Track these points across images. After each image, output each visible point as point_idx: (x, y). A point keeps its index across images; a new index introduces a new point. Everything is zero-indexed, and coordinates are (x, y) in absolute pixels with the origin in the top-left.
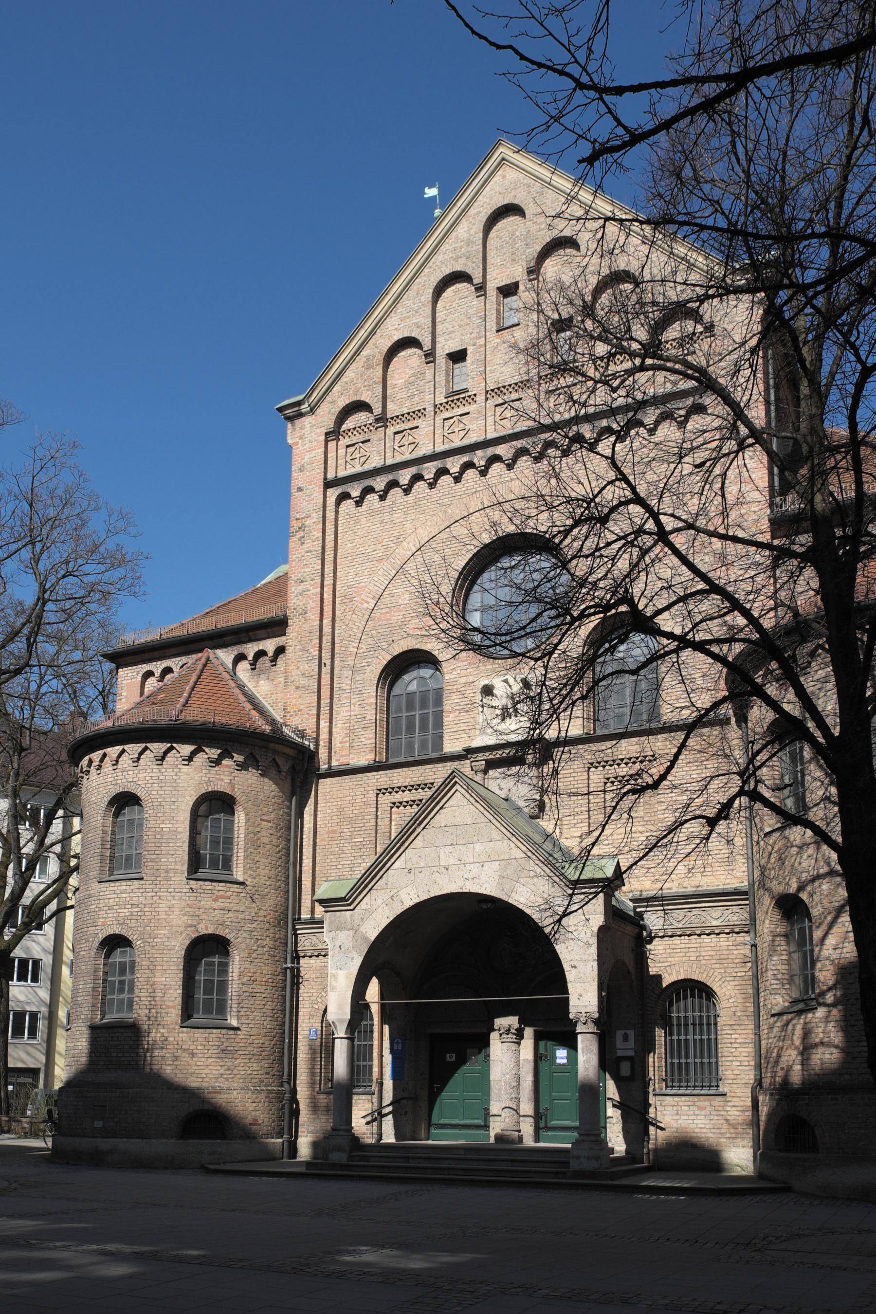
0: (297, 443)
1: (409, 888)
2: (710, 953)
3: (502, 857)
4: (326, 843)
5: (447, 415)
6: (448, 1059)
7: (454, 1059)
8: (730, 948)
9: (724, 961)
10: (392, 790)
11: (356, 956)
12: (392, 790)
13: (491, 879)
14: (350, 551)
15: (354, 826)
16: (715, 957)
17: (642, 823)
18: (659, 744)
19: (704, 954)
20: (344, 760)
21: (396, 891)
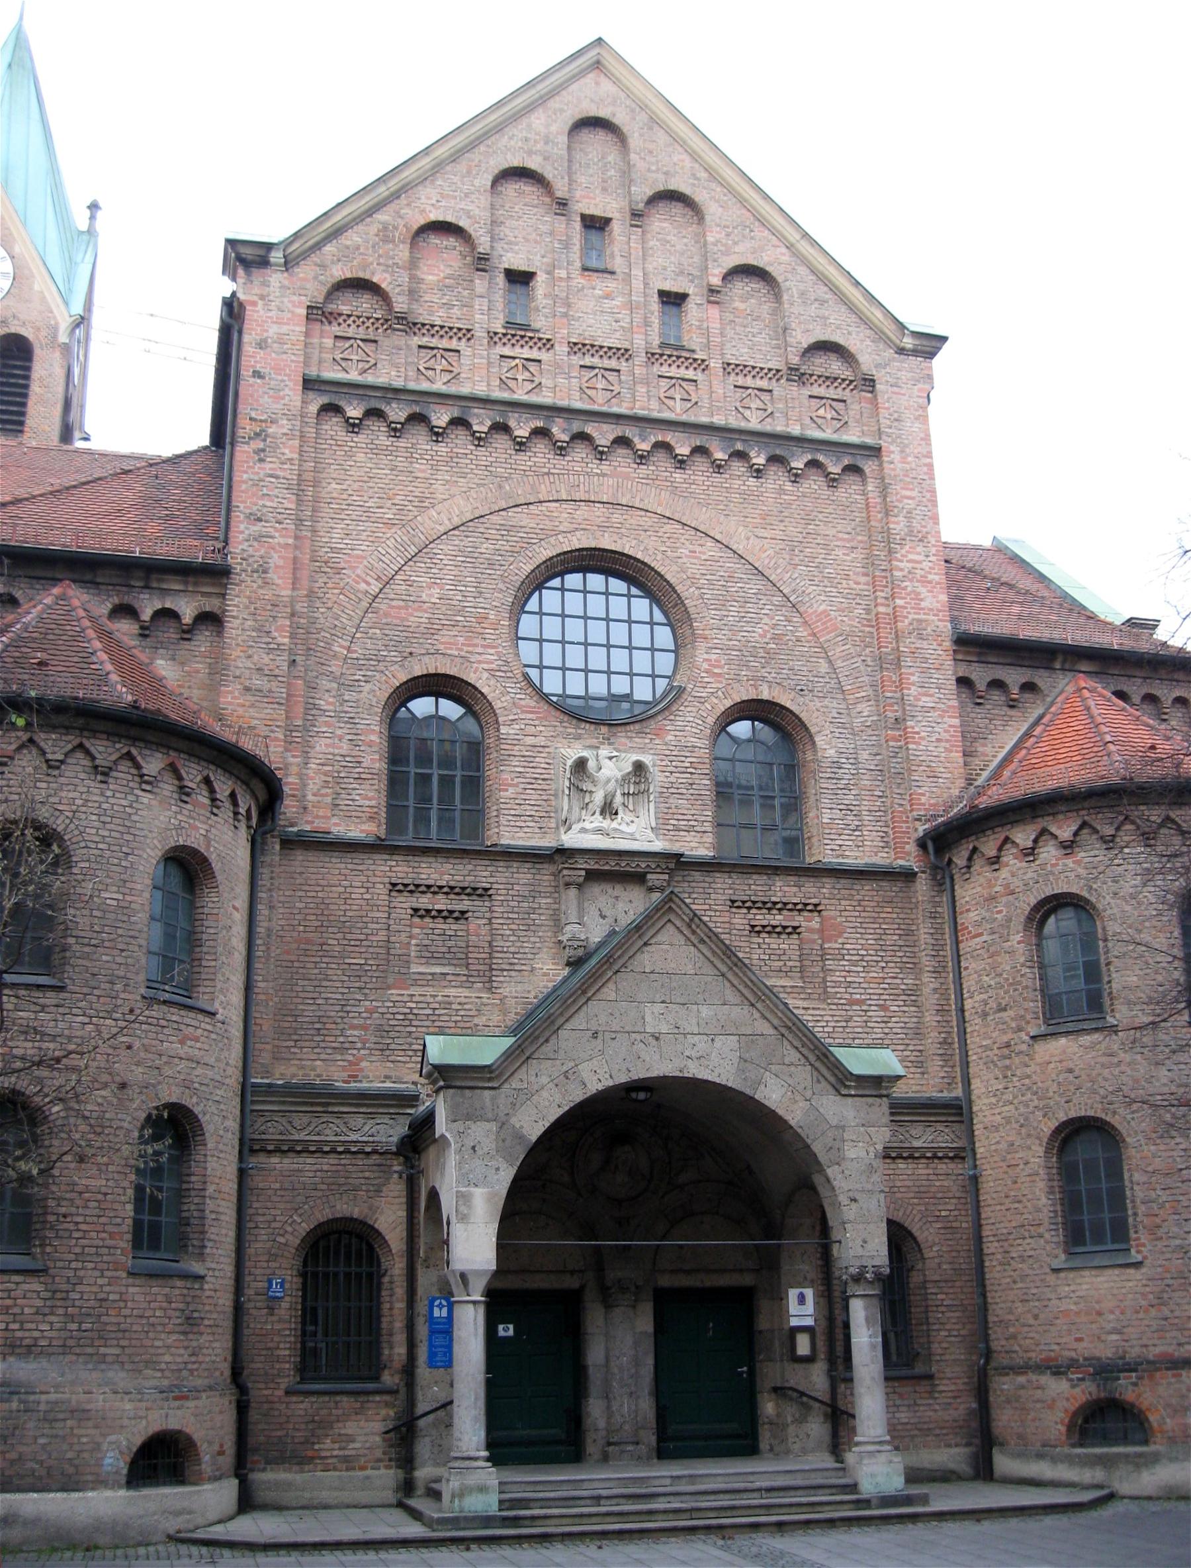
0: (254, 304)
2: (906, 1183)
3: (743, 1030)
4: (293, 958)
5: (507, 351)
6: (501, 1333)
7: (511, 1332)
8: (931, 1177)
10: (417, 889)
11: (503, 1165)
12: (417, 889)
13: (727, 1061)
14: (335, 495)
15: (348, 936)
17: (802, 996)
19: (899, 1184)
20: (320, 824)
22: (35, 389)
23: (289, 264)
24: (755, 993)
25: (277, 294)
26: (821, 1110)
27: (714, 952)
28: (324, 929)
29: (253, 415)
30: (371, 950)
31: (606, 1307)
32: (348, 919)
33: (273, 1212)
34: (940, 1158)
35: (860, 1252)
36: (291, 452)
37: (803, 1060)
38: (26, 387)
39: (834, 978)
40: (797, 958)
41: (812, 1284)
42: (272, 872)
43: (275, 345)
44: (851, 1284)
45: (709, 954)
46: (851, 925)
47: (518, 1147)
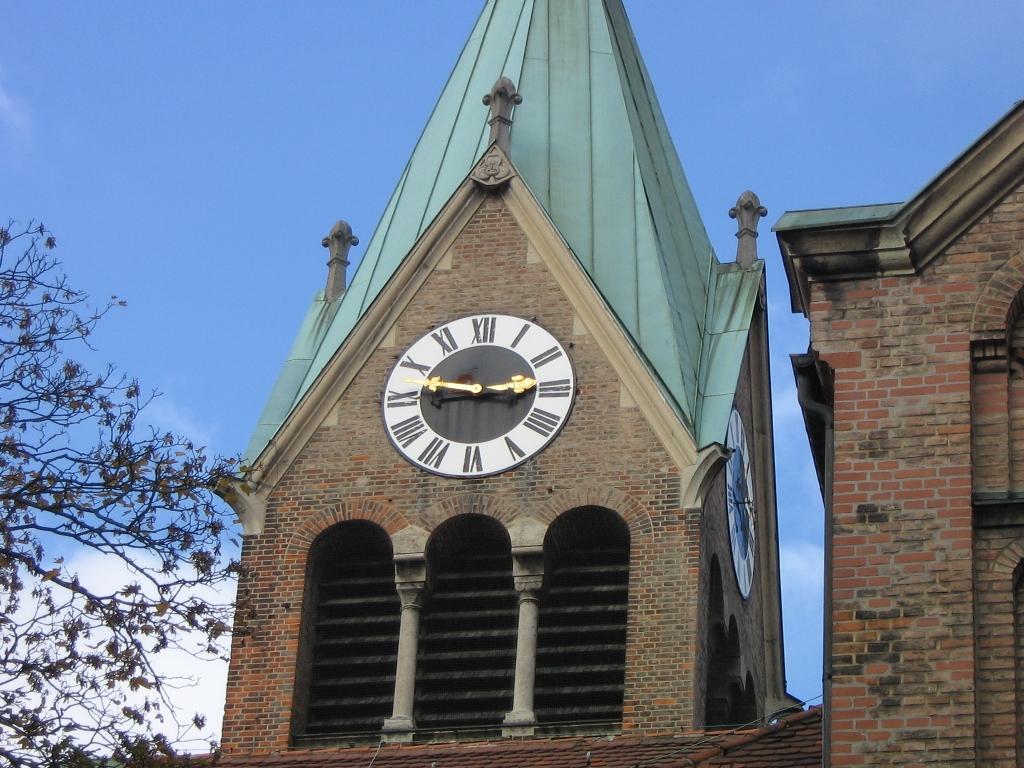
0: (852, 360)
22: (641, 618)
23: (920, 260)
25: (901, 329)
29: (865, 607)
36: (956, 676)
38: (622, 617)
43: (905, 443)
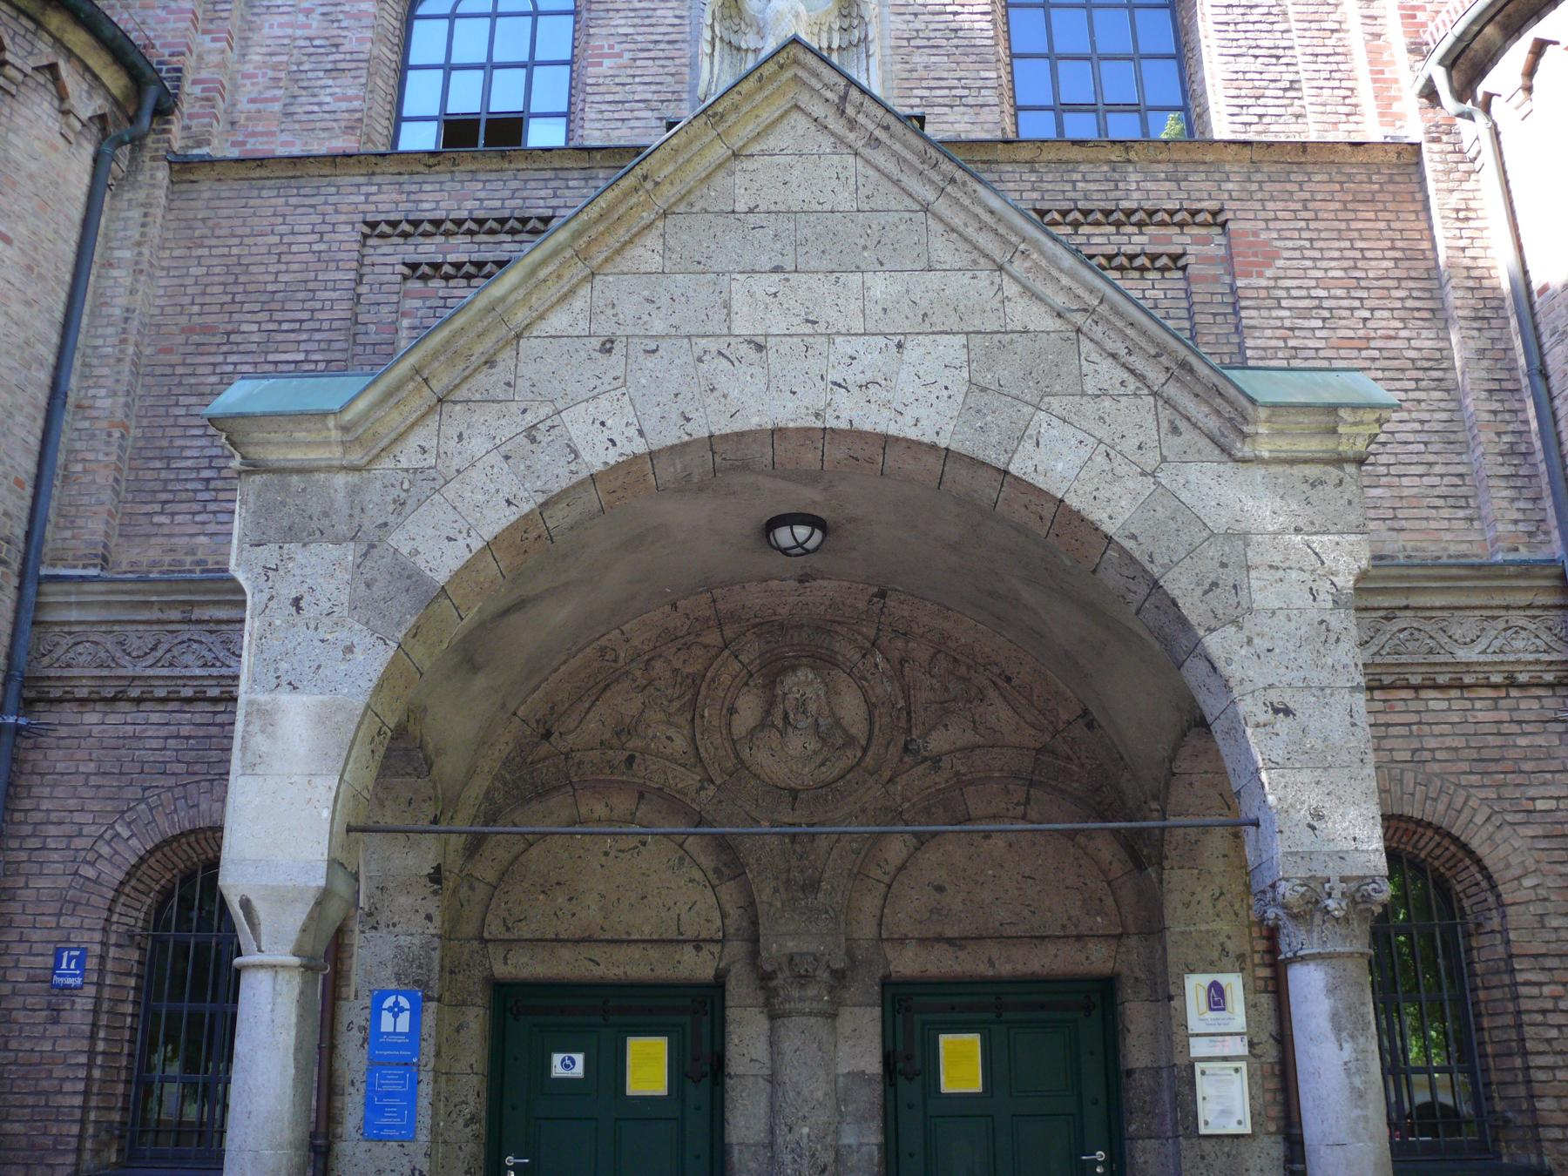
1: (604, 402)
2: (1449, 742)
3: (977, 324)
4: (175, 359)
6: (558, 1070)
7: (578, 1070)
8: (1505, 728)
9: (1493, 767)
12: (414, 228)
15: (278, 316)
16: (1467, 753)
18: (1230, 186)
21: (547, 410)
24: (1006, 242)
26: (1184, 496)
27: (901, 160)
28: (237, 307)
30: (317, 336)
31: (773, 1017)
32: (281, 287)
33: (78, 817)
34: (1522, 686)
35: (1306, 841)
37: (1132, 384)
39: (1260, 343)
40: (1184, 314)
41: (1240, 962)
42: (146, 215)
44: (1288, 927)
45: (891, 167)
46: (1290, 244)
47: (404, 598)
